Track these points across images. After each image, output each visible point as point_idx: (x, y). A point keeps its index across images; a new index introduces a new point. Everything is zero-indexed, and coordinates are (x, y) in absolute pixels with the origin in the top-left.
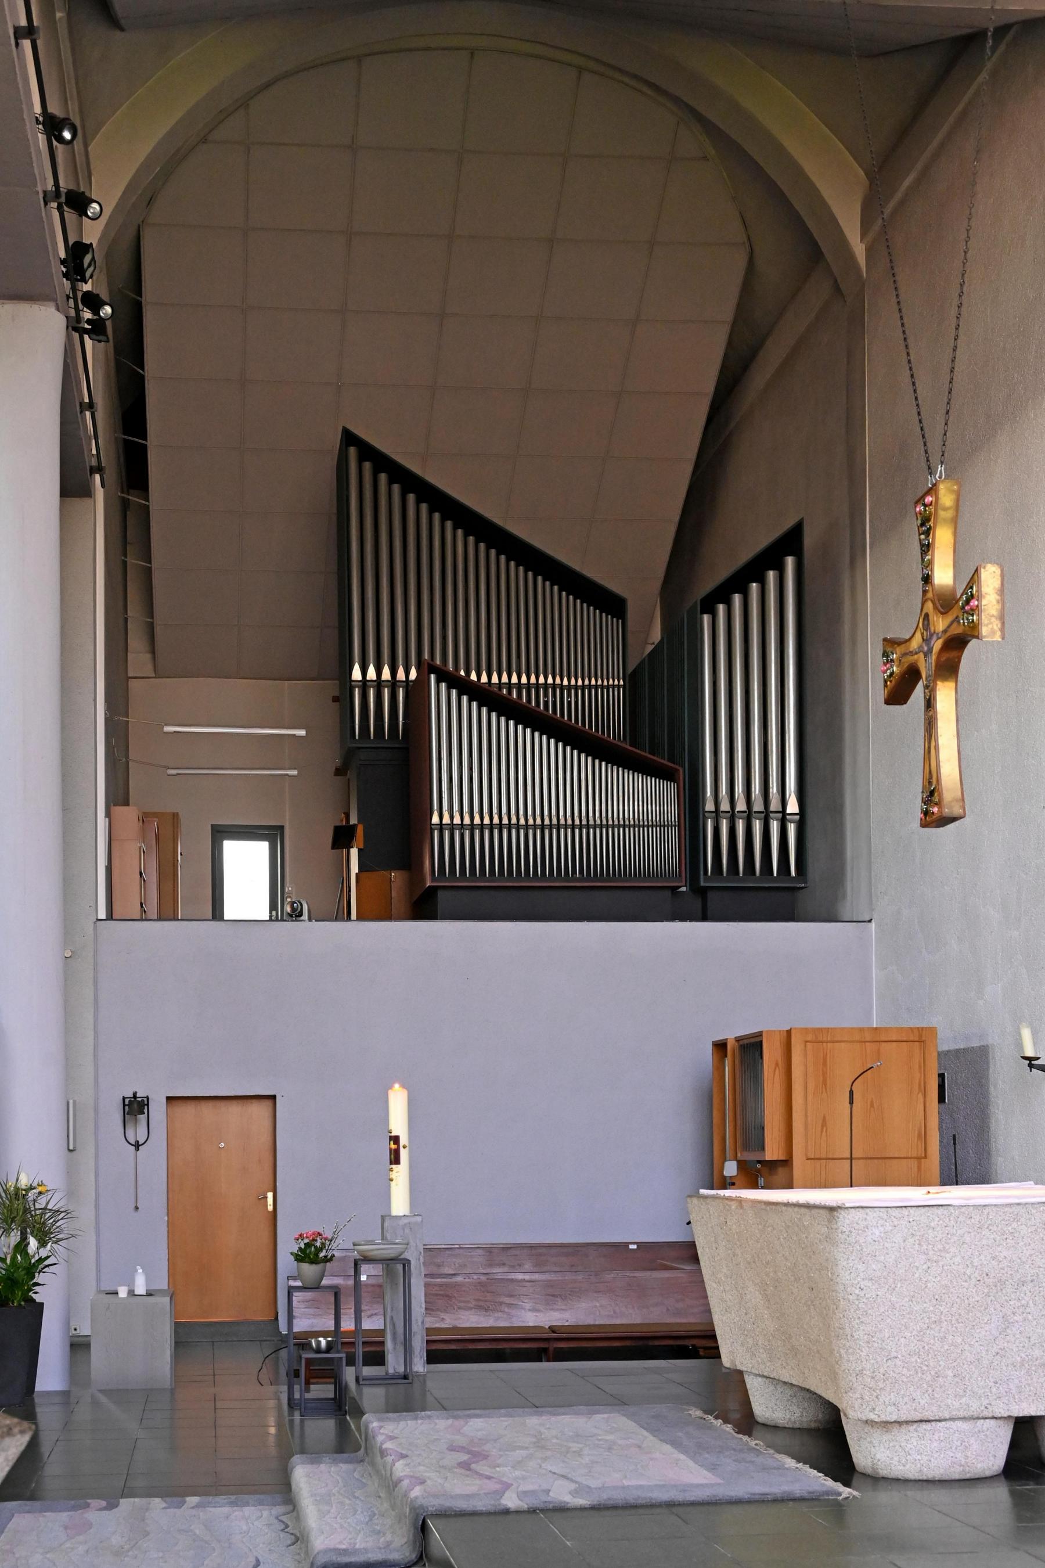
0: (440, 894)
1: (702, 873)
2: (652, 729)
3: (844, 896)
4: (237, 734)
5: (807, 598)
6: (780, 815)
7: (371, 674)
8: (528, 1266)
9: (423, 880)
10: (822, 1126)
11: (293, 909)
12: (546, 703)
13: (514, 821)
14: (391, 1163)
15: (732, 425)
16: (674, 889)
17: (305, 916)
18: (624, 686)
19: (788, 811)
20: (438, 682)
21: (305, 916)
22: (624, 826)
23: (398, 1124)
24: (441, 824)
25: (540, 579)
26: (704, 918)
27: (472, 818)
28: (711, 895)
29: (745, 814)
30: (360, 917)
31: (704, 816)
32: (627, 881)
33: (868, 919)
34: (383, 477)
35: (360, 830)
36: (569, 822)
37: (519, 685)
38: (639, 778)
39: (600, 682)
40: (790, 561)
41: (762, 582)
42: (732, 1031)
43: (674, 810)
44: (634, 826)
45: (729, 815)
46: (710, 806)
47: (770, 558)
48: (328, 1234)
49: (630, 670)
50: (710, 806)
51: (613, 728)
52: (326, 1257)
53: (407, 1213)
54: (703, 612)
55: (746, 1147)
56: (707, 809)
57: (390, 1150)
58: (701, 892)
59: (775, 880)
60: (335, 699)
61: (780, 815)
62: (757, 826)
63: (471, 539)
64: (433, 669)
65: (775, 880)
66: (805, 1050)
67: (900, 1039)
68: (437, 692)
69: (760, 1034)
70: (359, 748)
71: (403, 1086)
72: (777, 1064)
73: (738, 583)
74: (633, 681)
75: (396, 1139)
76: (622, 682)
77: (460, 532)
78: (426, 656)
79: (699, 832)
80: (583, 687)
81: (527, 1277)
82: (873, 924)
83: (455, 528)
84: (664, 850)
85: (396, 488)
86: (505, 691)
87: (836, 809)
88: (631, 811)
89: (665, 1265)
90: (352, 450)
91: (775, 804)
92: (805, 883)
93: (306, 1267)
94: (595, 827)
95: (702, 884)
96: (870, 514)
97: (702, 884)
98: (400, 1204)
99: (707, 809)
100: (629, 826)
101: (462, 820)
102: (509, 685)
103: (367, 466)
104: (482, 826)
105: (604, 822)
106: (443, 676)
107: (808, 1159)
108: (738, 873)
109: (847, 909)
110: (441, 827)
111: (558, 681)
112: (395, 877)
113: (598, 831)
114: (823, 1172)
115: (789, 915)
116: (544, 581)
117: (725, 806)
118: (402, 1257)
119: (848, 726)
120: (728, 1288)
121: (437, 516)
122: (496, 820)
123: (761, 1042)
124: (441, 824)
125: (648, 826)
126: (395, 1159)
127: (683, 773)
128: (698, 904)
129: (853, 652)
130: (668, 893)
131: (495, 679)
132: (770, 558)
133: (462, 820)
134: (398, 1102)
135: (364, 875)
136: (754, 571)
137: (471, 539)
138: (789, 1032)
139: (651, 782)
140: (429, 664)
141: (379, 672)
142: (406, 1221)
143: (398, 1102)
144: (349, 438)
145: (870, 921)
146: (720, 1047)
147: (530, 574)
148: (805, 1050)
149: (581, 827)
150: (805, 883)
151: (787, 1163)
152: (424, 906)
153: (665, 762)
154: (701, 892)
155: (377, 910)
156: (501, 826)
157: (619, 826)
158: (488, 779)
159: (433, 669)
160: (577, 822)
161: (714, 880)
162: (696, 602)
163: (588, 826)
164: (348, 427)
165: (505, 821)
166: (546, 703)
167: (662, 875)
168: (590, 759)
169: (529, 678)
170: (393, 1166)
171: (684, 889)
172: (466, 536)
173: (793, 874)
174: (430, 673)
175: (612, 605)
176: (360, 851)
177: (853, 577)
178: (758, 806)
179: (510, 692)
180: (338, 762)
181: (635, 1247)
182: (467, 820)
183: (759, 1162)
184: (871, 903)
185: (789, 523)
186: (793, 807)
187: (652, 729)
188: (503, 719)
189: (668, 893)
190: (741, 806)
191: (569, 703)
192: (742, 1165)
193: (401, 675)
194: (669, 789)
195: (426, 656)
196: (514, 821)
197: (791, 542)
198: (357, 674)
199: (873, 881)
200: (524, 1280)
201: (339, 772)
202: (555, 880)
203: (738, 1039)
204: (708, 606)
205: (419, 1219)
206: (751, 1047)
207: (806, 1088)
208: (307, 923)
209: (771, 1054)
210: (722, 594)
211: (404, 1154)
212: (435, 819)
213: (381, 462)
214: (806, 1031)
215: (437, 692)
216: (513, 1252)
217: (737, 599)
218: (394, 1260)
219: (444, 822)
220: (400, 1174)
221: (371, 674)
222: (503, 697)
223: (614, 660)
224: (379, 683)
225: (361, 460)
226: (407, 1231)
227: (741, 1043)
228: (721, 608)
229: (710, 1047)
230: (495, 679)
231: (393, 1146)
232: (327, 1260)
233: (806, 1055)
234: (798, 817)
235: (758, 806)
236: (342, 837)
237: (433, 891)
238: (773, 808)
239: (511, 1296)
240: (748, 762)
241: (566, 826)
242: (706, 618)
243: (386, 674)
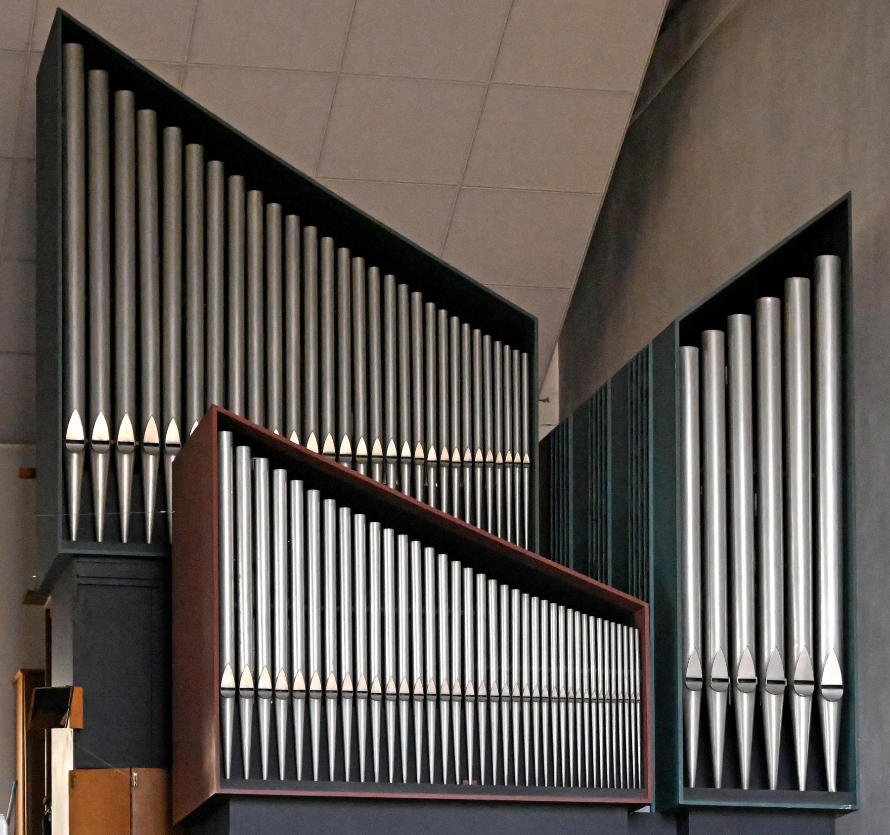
0: (234, 808)
1: (681, 782)
4: (654, 400)
6: (811, 688)
12: (426, 490)
15: (706, 34)
16: (632, 808)
18: (531, 465)
19: (824, 682)
20: (236, 443)
22: (550, 700)
25: (390, 279)
35: (78, 695)
38: (575, 618)
40: (828, 264)
46: (694, 670)
50: (694, 670)
51: (515, 533)
54: (683, 343)
56: (689, 674)
60: (30, 474)
61: (811, 688)
63: (274, 207)
64: (226, 422)
76: (527, 459)
77: (255, 196)
88: (563, 676)
90: (74, 50)
91: (802, 669)
94: (541, 699)
95: (682, 801)
99: (689, 674)
102: (354, 458)
103: (98, 76)
104: (273, 693)
105: (516, 693)
106: (243, 435)
108: (796, 786)
111: (419, 453)
112: (139, 779)
116: (397, 282)
117: (719, 670)
121: (216, 166)
122: (316, 685)
125: (590, 701)
135: (84, 774)
136: (768, 277)
137: (274, 208)
140: (219, 413)
144: (68, 29)
147: (374, 270)
149: (511, 699)
150: (854, 802)
157: (541, 699)
159: (226, 422)
162: (672, 325)
163: (521, 699)
164: (63, 8)
166: (426, 490)
167: (614, 786)
171: (646, 810)
172: (266, 202)
173: (832, 786)
174: (221, 428)
175: (510, 327)
178: (774, 671)
180: (36, 577)
186: (832, 674)
188: (345, 512)
189: (623, 815)
190: (746, 670)
191: (438, 491)
194: (624, 638)
195: (216, 399)
197: (829, 231)
198: (75, 430)
201: (33, 597)
202: (433, 790)
204: (692, 331)
210: (714, 314)
212: (228, 680)
213: (123, 73)
215: (235, 465)
217: (740, 322)
223: (515, 421)
225: (88, 66)
234: (840, 692)
235: (774, 671)
236: (47, 708)
237: (222, 801)
238: (798, 675)
242: (689, 353)
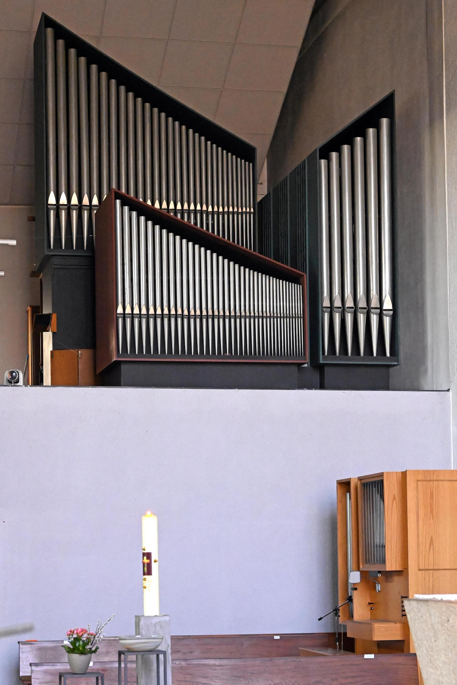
1: (321, 353)
2: (280, 244)
3: (426, 370)
5: (398, 148)
6: (378, 311)
7: (63, 200)
8: (197, 654)
9: (110, 357)
10: (430, 545)
11: (13, 378)
13: (179, 312)
14: (144, 574)
17: (21, 383)
19: (385, 307)
20: (122, 205)
21: (21, 383)
23: (150, 544)
24: (124, 313)
26: (322, 387)
27: (148, 310)
28: (326, 369)
29: (353, 310)
30: (54, 384)
31: (322, 310)
32: (265, 359)
33: (447, 389)
34: (73, 51)
35: (54, 317)
36: (221, 313)
37: (189, 211)
38: (273, 281)
39: (236, 210)
40: (385, 122)
41: (364, 136)
42: (353, 474)
43: (300, 305)
44: (277, 317)
45: (340, 310)
46: (326, 303)
47: (370, 119)
48: (93, 631)
49: (259, 198)
50: (326, 303)
51: (247, 242)
52: (90, 649)
53: (158, 614)
54: (321, 158)
55: (367, 561)
56: (324, 305)
57: (144, 564)
58: (320, 368)
59: (375, 359)
62: (362, 318)
63: (139, 100)
64: (118, 196)
65: (375, 359)
66: (417, 487)
67: (451, 479)
68: (122, 215)
69: (382, 475)
70: (54, 255)
71: (154, 514)
72: (394, 498)
73: (346, 137)
74: (261, 208)
75: (148, 555)
76: (252, 210)
78: (114, 186)
79: (318, 323)
80: (233, 213)
81: (217, 662)
82: (451, 393)
83: (127, 91)
84: (292, 334)
85: (83, 60)
86: (179, 216)
87: (419, 307)
89: (309, 652)
90: (50, 31)
91: (374, 302)
92: (398, 361)
93: (76, 657)
94: (267, 317)
95: (321, 361)
96: (446, 88)
97: (321, 361)
98: (151, 606)
99: (324, 305)
100: (267, 317)
101: (267, 315)
103: (61, 42)
105: (261, 314)
106: (125, 201)
107: (419, 570)
109: (427, 382)
110: (124, 315)
111: (204, 208)
113: (252, 320)
114: (431, 580)
115: (385, 386)
118: (158, 649)
119: (428, 245)
120: (444, 672)
123: (382, 481)
124: (124, 313)
126: (149, 572)
127: (306, 279)
128: (316, 377)
129: (433, 189)
130: (295, 368)
131: (164, 206)
132: (370, 119)
133: (267, 315)
134: (150, 527)
135: (57, 352)
136: (358, 128)
138: (404, 474)
139: (283, 284)
140: (116, 193)
141: (69, 199)
142: (157, 620)
143: (150, 527)
144: (47, 21)
145: (448, 390)
146: (345, 485)
148: (417, 487)
150: (398, 361)
151: (402, 573)
152: (107, 375)
153: (289, 268)
154: (320, 368)
155: (66, 378)
156: (176, 316)
158: (160, 280)
159: (118, 196)
160: (279, 315)
161: (329, 359)
162: (316, 150)
163: (213, 317)
165: (173, 312)
167: (290, 355)
168: (237, 266)
169: (182, 206)
170: (146, 577)
171: (306, 365)
173: (388, 354)
174: (116, 198)
175: (245, 152)
176: (54, 334)
177: (432, 133)
178: (362, 303)
179: (176, 215)
181: (278, 637)
182: (144, 311)
183: (380, 572)
184: (449, 377)
185: (386, 93)
186: (388, 304)
187: (280, 244)
188: (171, 235)
192: (364, 575)
193: (86, 201)
195: (114, 186)
196: (179, 312)
197: (385, 107)
198: (52, 200)
199: (450, 360)
200: (215, 665)
201: (34, 274)
203: (360, 479)
204: (325, 153)
205: (167, 618)
206: (373, 486)
207: (418, 516)
208: (24, 388)
209: (391, 489)
210: (334, 145)
211: (155, 567)
212: (120, 310)
214: (417, 472)
215: (122, 215)
216: (186, 642)
218: (151, 651)
219: (126, 312)
220: (152, 582)
221: (63, 200)
222: (170, 217)
224: (189, 211)
226: (158, 628)
227: (363, 481)
228: (334, 155)
229: (335, 485)
230: (164, 206)
231: (146, 561)
232: (91, 652)
233: (417, 491)
235: (362, 303)
236: (40, 323)
239: (205, 677)
240: (354, 271)
241: (195, 317)
242: (323, 162)
243: (75, 200)
